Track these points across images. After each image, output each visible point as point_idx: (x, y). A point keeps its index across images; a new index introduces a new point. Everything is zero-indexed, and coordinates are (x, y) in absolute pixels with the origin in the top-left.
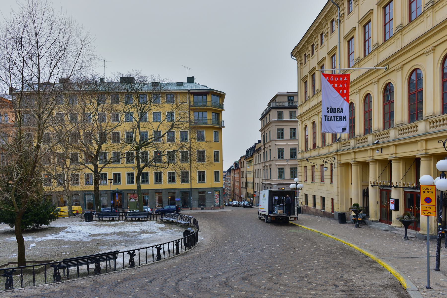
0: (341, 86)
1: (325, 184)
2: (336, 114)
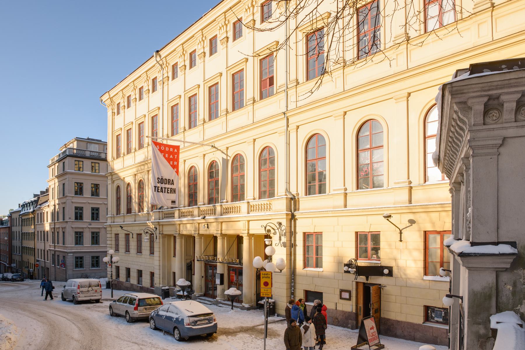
0: (171, 157)
1: (143, 256)
2: (167, 186)
